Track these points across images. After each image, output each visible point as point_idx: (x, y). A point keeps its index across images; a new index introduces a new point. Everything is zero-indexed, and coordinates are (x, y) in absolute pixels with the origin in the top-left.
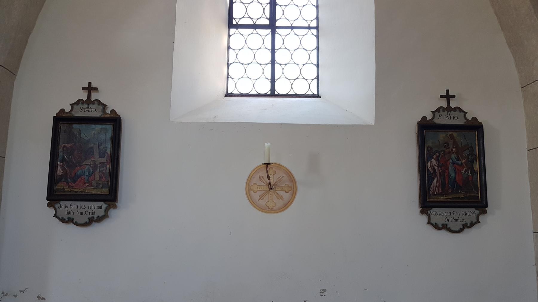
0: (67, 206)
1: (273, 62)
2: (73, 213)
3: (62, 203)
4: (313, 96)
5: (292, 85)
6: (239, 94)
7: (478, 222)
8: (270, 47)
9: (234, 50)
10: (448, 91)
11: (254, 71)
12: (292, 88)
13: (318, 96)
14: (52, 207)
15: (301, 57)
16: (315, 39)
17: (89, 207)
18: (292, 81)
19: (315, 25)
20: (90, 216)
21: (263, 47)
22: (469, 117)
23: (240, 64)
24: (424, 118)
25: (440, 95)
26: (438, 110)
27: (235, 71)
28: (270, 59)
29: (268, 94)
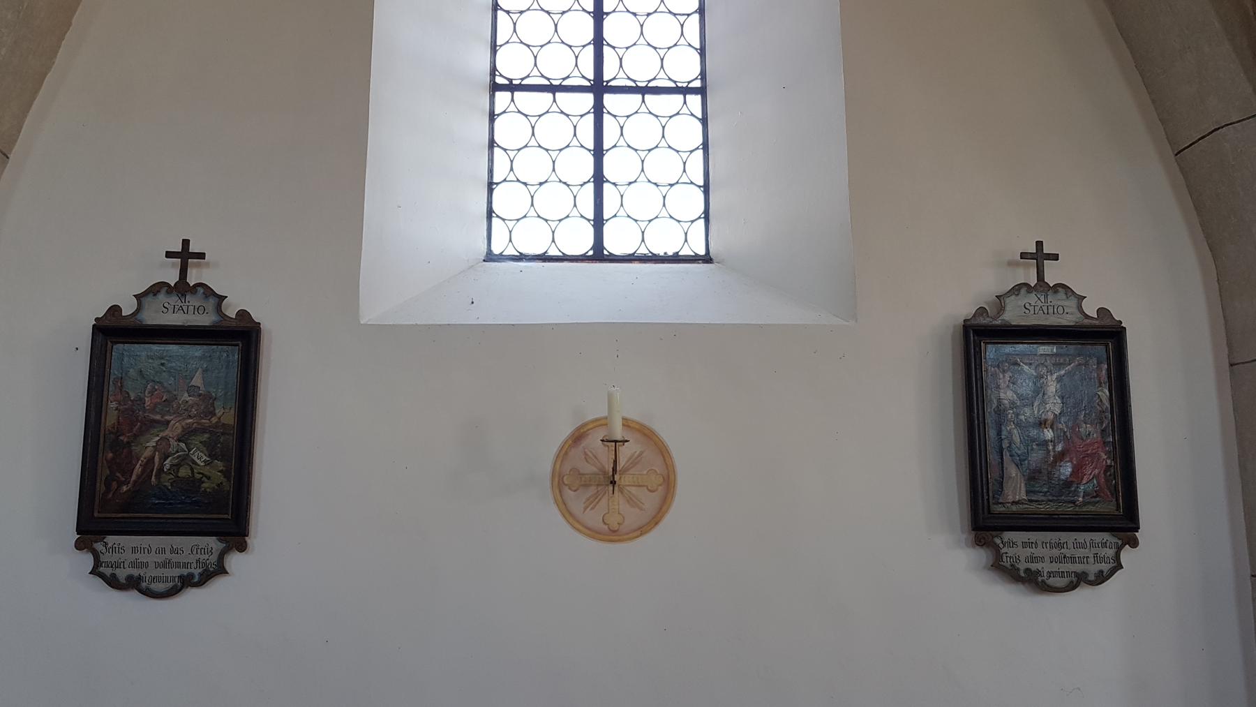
0: (1017, 544)
1: (599, 179)
2: (189, 565)
3: (111, 539)
4: (694, 259)
5: (643, 233)
6: (517, 256)
7: (221, 570)
8: (589, 142)
9: (505, 150)
10: (186, 243)
11: (554, 201)
12: (643, 240)
13: (707, 259)
14: (86, 550)
15: (664, 166)
16: (699, 126)
17: (199, 551)
18: (643, 225)
19: (498, 94)
20: (185, 572)
21: (663, 144)
22: (1091, 309)
23: (518, 183)
24: (115, 310)
25: (167, 252)
26: (156, 289)
27: (507, 200)
28: (591, 172)
29: (588, 256)
